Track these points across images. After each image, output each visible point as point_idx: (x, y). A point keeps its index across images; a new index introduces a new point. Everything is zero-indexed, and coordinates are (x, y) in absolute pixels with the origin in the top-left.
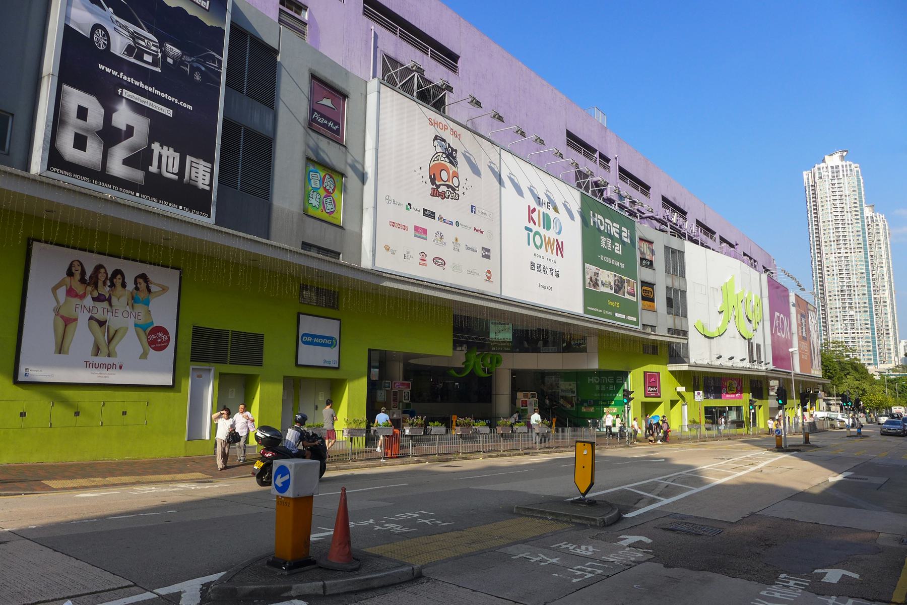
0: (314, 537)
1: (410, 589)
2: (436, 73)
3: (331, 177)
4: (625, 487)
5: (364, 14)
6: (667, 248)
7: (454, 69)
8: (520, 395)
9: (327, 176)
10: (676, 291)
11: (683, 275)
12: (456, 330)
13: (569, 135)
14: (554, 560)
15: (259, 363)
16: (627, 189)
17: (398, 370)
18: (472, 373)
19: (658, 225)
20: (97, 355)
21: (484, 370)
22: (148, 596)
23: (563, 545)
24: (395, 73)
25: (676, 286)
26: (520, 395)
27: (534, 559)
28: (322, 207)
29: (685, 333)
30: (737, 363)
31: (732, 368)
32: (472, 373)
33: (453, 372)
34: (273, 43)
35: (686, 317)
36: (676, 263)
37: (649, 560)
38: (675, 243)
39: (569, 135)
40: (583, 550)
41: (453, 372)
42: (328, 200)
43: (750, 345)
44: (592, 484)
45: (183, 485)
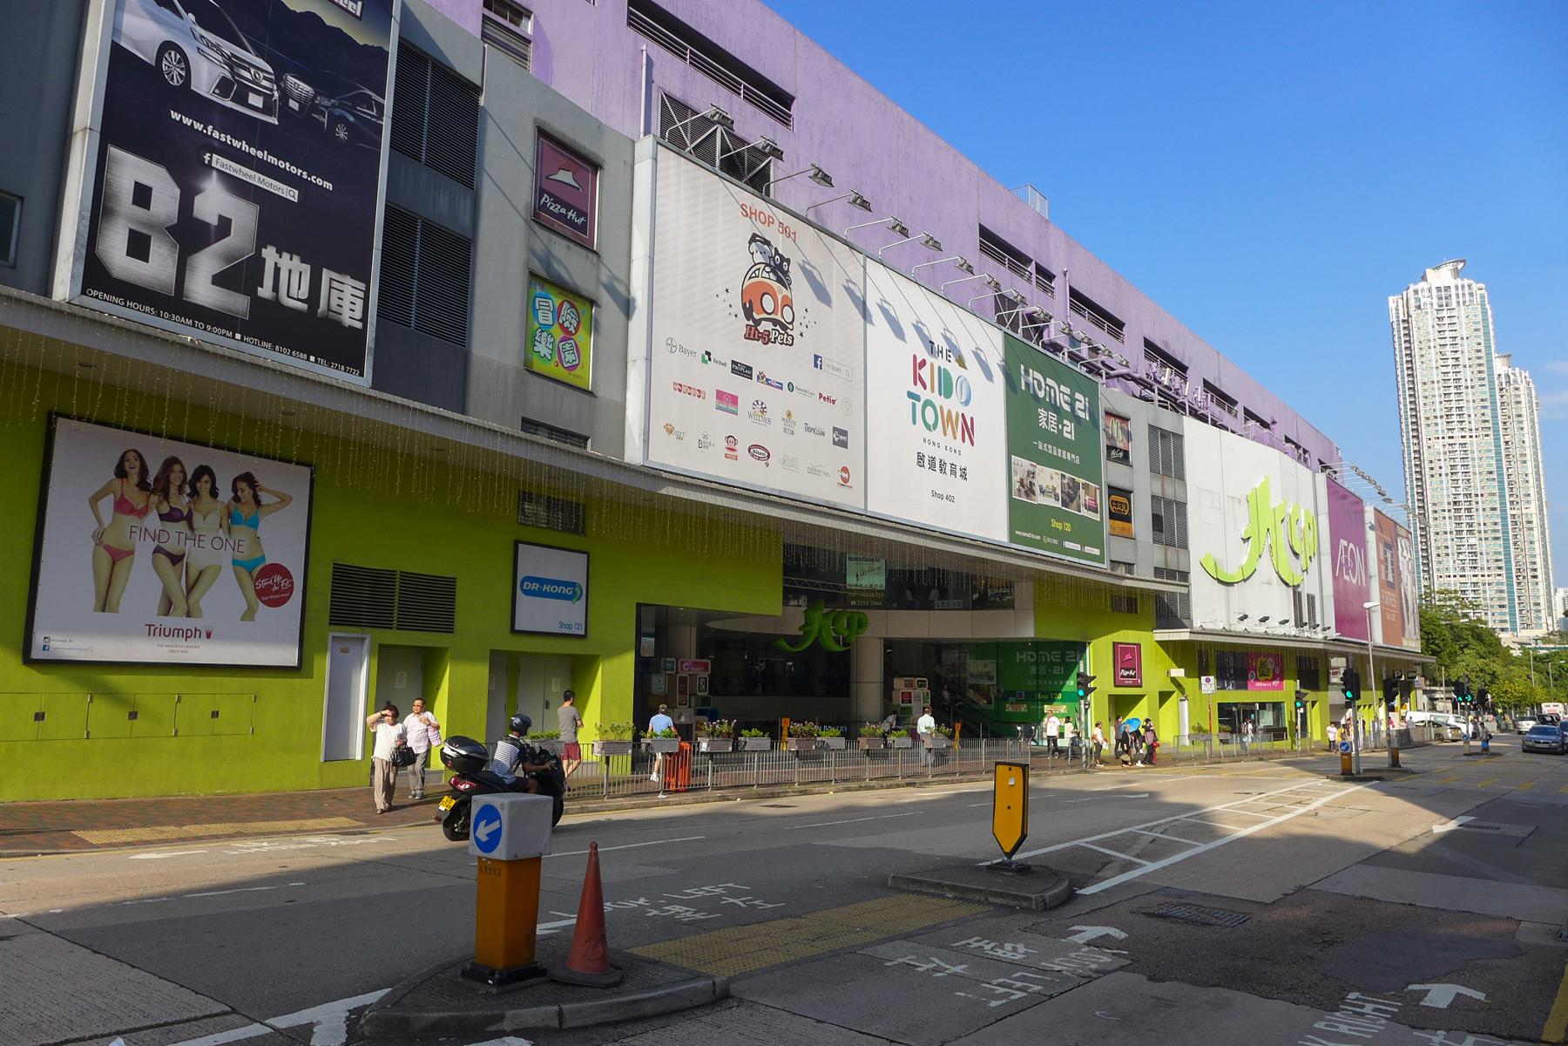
0: (542, 929)
1: (709, 1019)
2: (754, 126)
3: (573, 306)
4: (1081, 842)
5: (629, 24)
6: (1153, 429)
7: (785, 119)
8: (899, 683)
9: (566, 305)
10: (1169, 503)
11: (1181, 476)
12: (789, 570)
13: (984, 233)
14: (958, 969)
15: (448, 627)
16: (1083, 326)
17: (688, 640)
18: (817, 644)
19: (1137, 389)
20: (167, 614)
21: (837, 640)
22: (256, 1030)
23: (974, 943)
24: (684, 127)
25: (1169, 494)
26: (899, 683)
27: (924, 967)
28: (556, 358)
29: (1184, 576)
30: (1274, 628)
31: (1266, 636)
32: (817, 644)
33: (783, 644)
34: (472, 75)
35: (1186, 547)
36: (1168, 454)
37: (1122, 968)
38: (1167, 420)
39: (984, 233)
40: (1007, 952)
41: (783, 644)
42: (567, 347)
43: (1297, 596)
44: (1023, 837)
45: (316, 839)
